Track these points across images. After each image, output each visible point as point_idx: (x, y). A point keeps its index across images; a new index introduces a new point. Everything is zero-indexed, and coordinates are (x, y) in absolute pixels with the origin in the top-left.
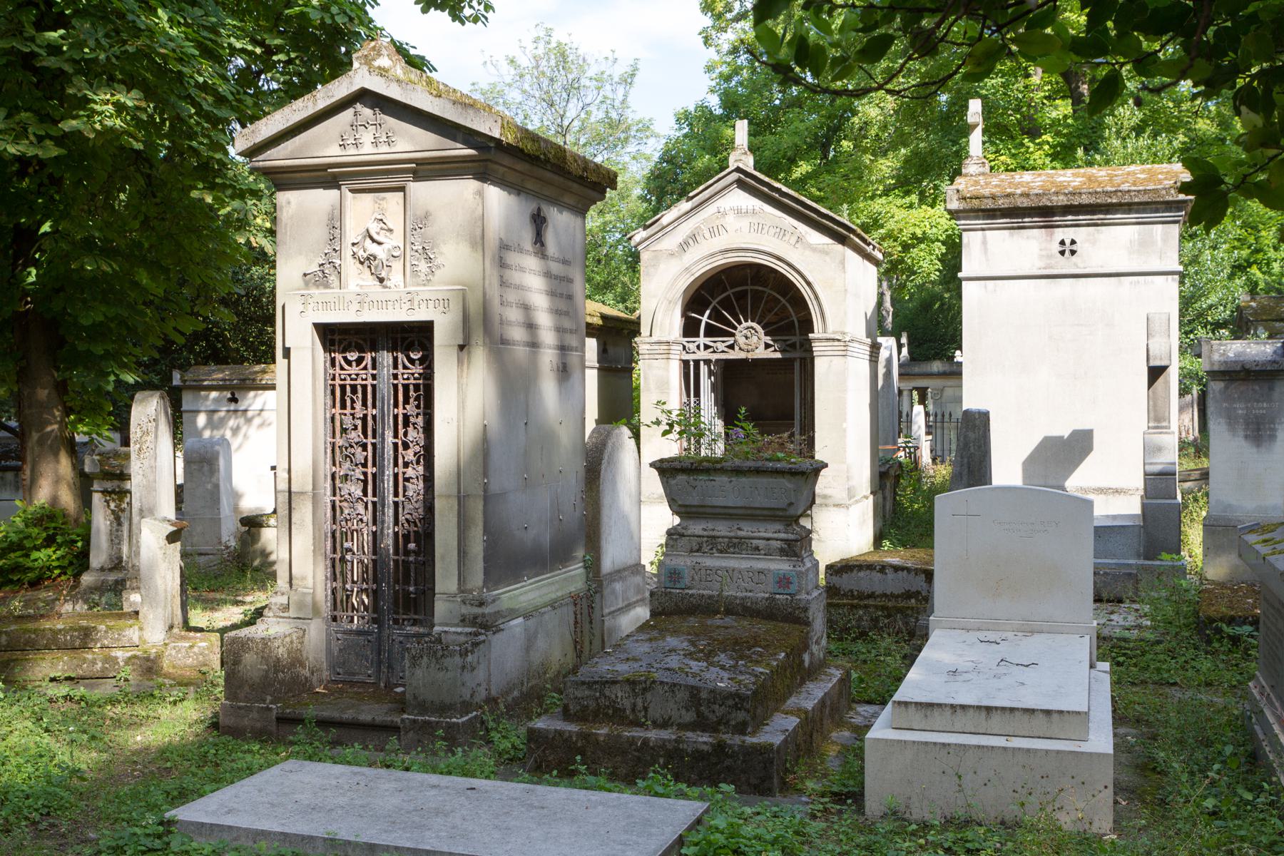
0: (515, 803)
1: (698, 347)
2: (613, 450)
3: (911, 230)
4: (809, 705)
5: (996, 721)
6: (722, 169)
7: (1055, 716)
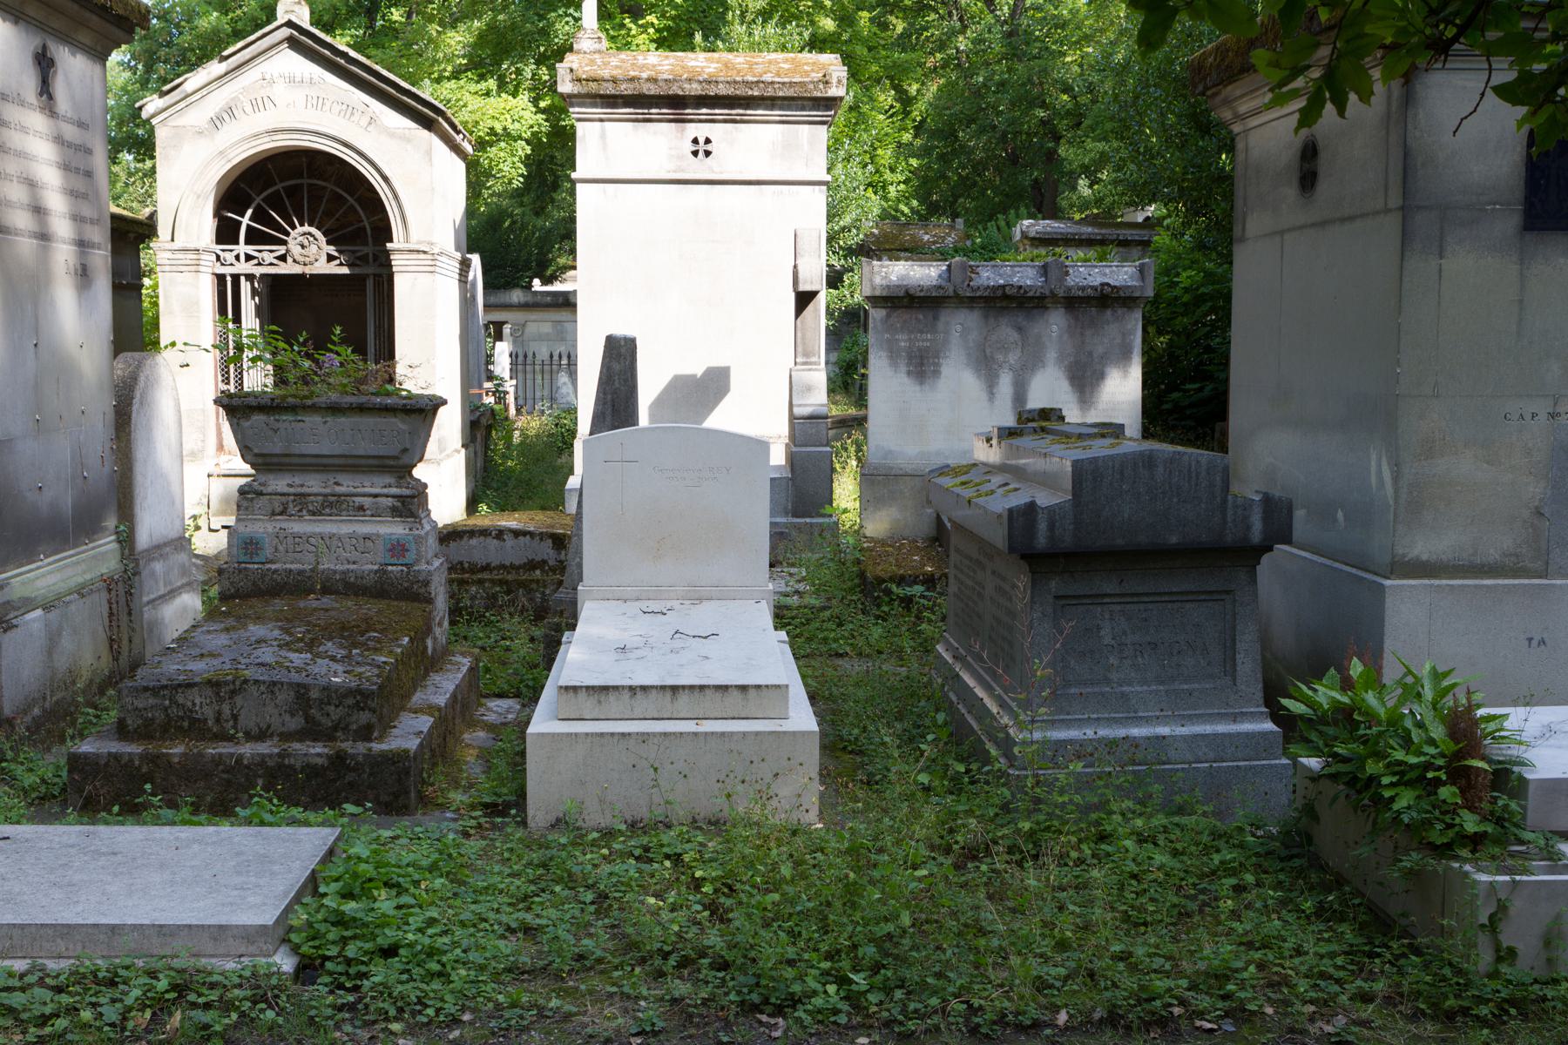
0: (72, 850)
1: (237, 258)
2: (146, 386)
3: (490, 123)
4: (441, 700)
5: (684, 703)
6: (269, 22)
7: (752, 692)
